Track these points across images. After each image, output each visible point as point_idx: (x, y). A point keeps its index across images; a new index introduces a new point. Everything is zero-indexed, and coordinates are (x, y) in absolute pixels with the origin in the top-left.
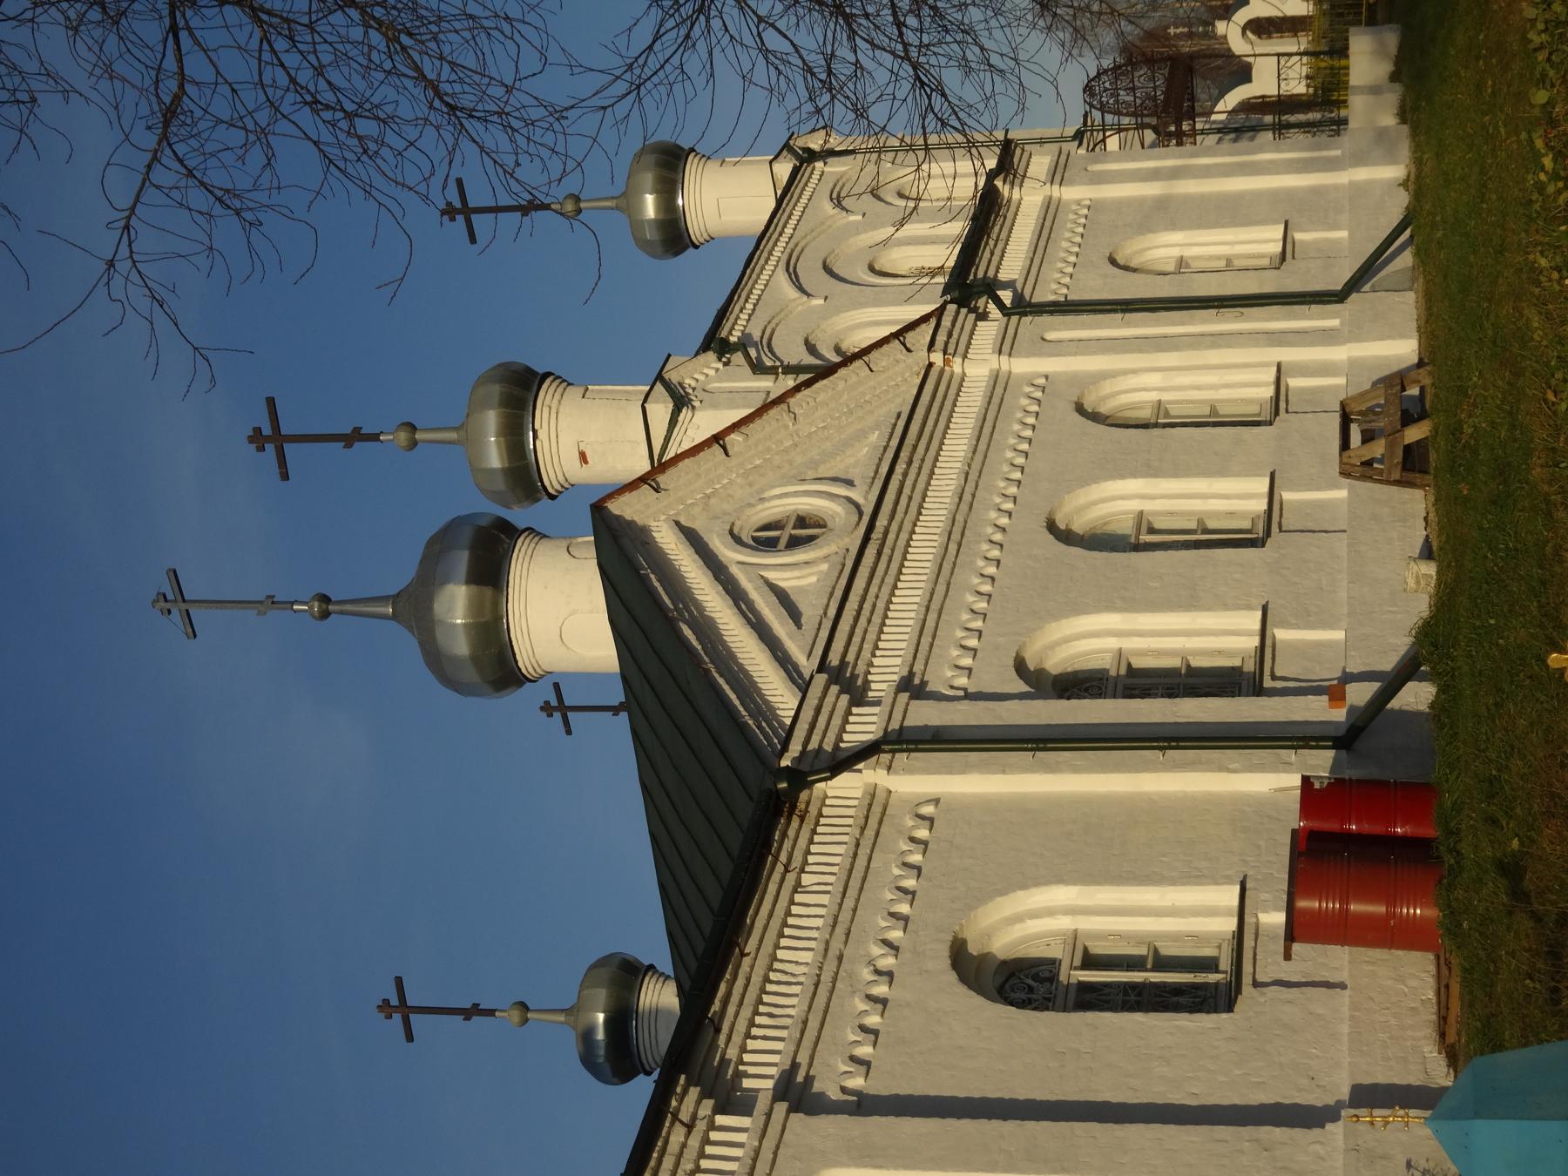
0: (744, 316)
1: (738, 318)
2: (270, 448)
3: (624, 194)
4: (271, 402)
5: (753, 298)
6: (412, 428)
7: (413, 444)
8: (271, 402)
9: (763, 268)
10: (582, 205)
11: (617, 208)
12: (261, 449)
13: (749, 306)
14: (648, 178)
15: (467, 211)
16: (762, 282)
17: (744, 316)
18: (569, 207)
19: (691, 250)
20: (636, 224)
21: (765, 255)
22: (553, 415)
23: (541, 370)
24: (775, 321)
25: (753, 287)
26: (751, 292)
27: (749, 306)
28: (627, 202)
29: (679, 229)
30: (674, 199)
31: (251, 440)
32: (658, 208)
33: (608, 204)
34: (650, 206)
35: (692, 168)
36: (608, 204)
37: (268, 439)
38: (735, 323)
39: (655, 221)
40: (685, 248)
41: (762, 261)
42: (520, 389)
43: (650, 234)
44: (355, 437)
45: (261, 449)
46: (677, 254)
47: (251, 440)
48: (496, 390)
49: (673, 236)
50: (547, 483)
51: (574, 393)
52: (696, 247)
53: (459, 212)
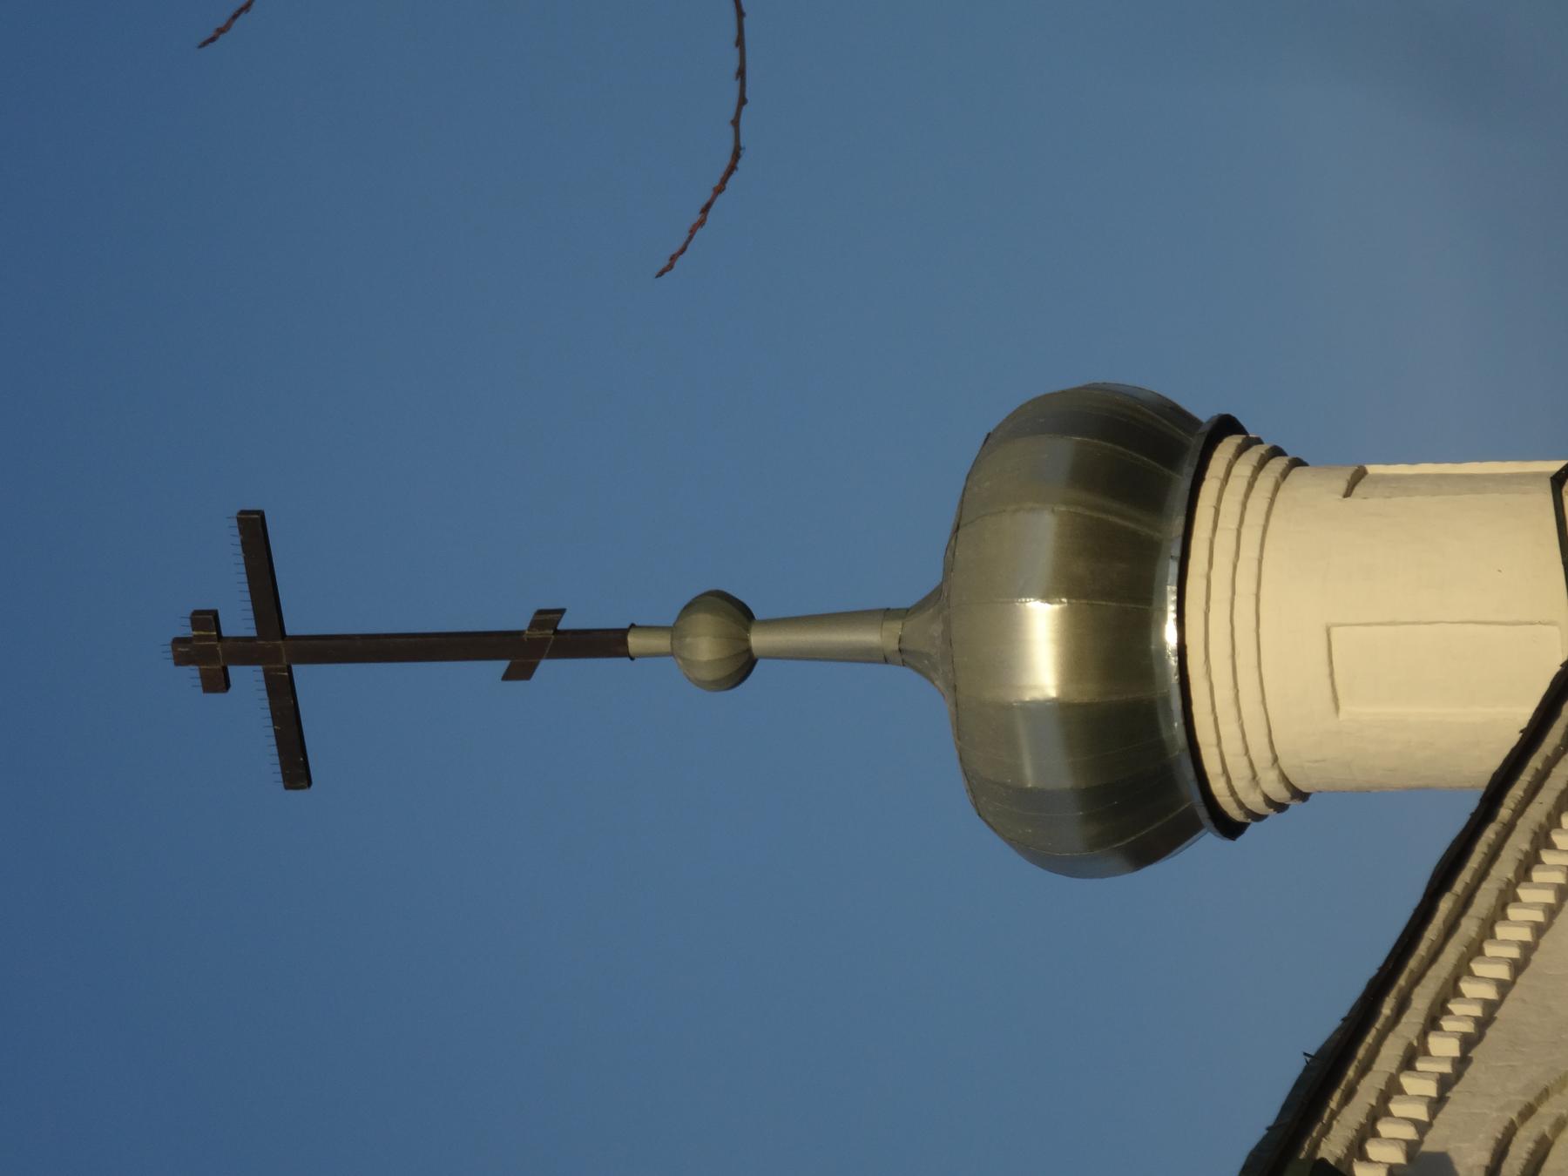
0: (1420, 1085)
1: (1394, 1088)
2: (248, 680)
3: (935, 600)
4: (253, 529)
5: (1463, 1014)
6: (742, 615)
7: (743, 666)
8: (253, 529)
9: (1508, 896)
10: (759, 640)
11: (904, 656)
12: (217, 682)
13: (1444, 1047)
14: (1040, 532)
15: (278, 650)
16: (1490, 968)
17: (1420, 1085)
18: (705, 645)
19: (1208, 842)
20: (981, 720)
21: (1519, 842)
22: (1251, 536)
23: (1205, 412)
24: (1547, 1113)
25: (1462, 969)
26: (1452, 989)
27: (1444, 1047)
28: (945, 635)
29: (1161, 748)
30: (1142, 624)
31: (184, 652)
32: (1075, 662)
33: (870, 637)
34: (1041, 648)
35: (1227, 498)
36: (870, 637)
37: (244, 652)
38: (1379, 1111)
39: (1061, 709)
40: (1183, 831)
41: (1505, 868)
42: (1135, 477)
43: (1045, 767)
44: (529, 647)
45: (217, 682)
46: (1144, 854)
47: (184, 652)
48: (1059, 451)
49: (1137, 778)
50: (1218, 787)
51: (1313, 492)
52: (1231, 829)
53: (244, 652)
